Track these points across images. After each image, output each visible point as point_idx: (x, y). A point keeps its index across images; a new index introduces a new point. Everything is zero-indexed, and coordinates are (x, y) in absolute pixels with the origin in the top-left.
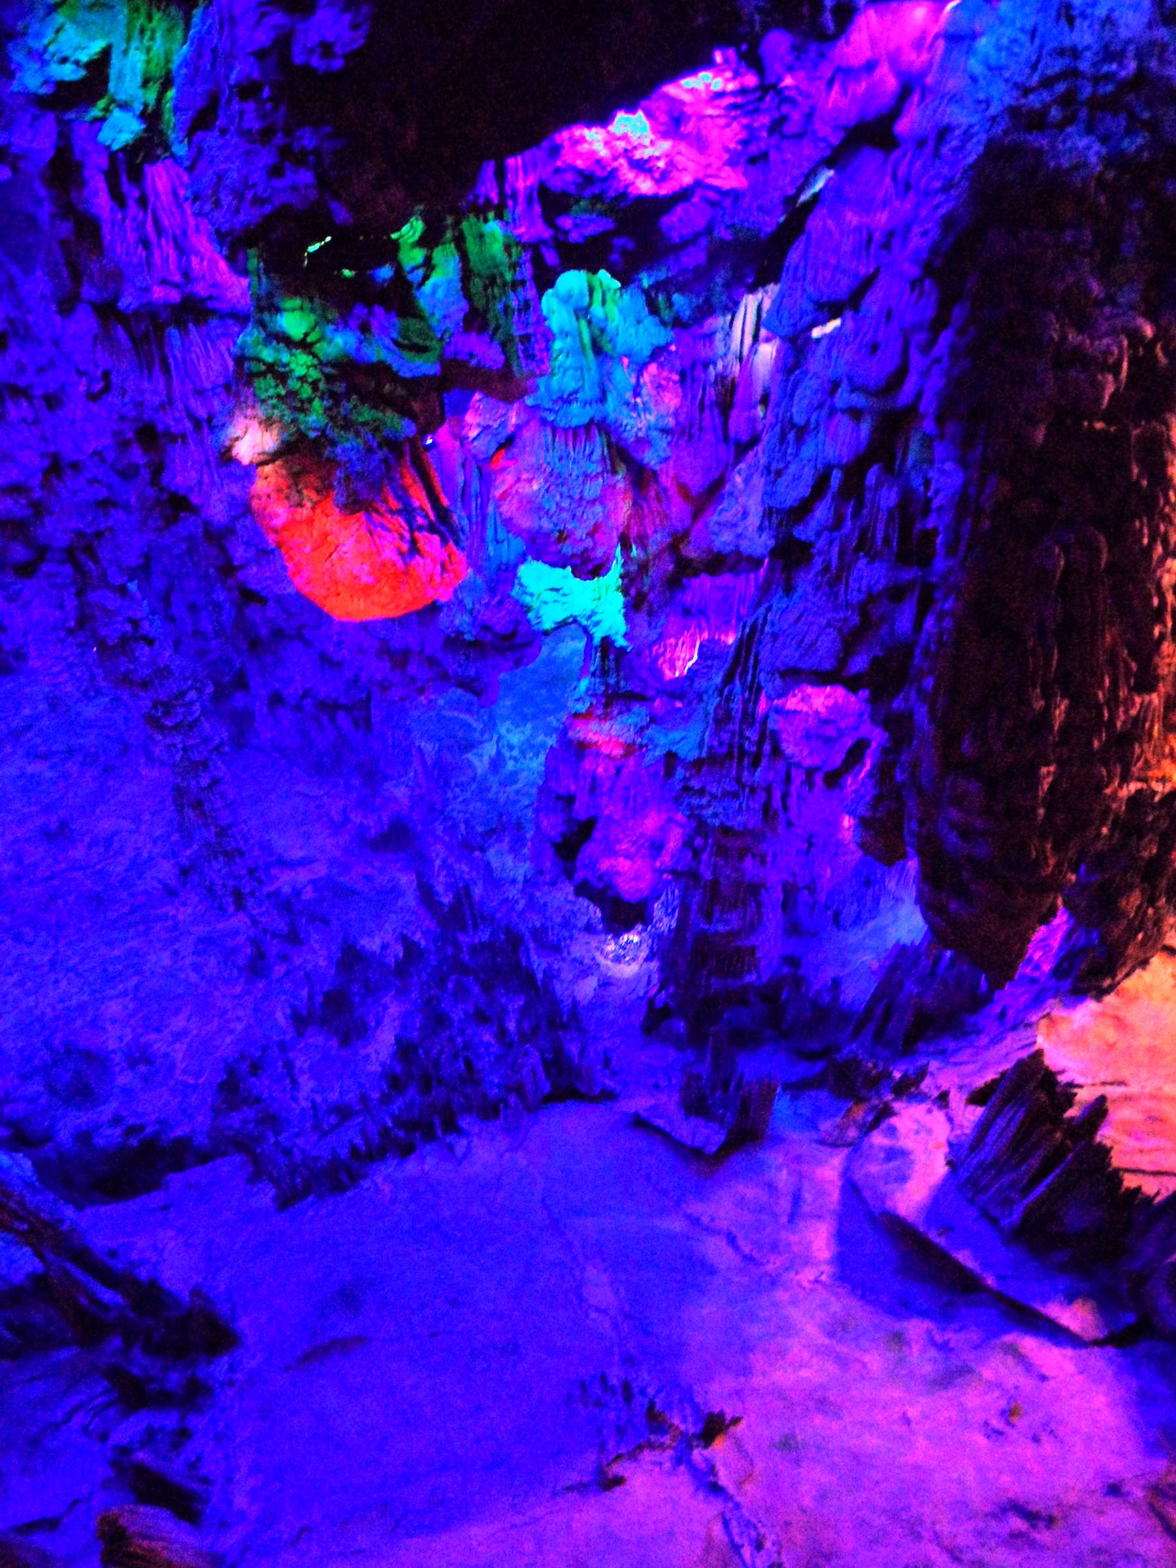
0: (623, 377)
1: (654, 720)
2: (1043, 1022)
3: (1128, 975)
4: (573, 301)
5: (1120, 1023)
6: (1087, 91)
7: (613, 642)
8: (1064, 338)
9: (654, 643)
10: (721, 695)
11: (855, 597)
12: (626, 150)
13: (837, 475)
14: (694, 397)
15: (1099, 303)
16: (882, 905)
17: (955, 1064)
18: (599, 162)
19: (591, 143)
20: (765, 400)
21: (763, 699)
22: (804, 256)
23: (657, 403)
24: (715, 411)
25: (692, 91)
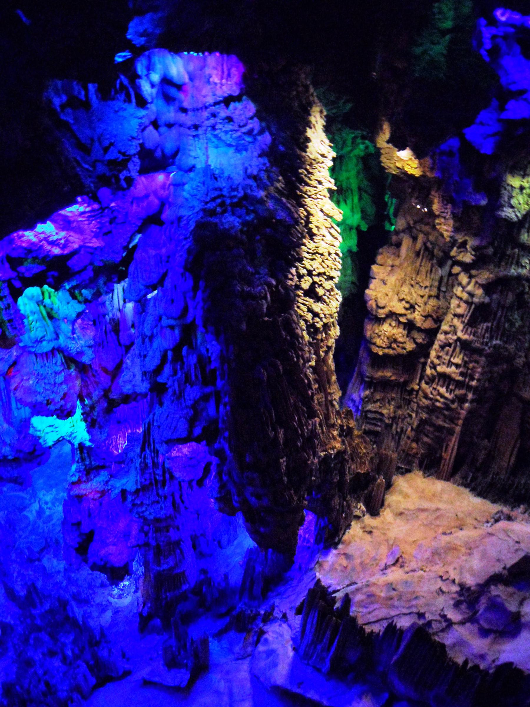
0: (66, 328)
1: (112, 476)
2: (317, 566)
3: (344, 534)
4: (35, 298)
5: (348, 556)
6: (228, 201)
7: (84, 444)
8: (243, 290)
9: (105, 440)
10: (141, 457)
11: (189, 403)
12: (45, 238)
13: (170, 353)
14: (102, 330)
15: (253, 274)
16: (238, 532)
17: (286, 598)
18: (33, 243)
19: (28, 236)
20: (133, 326)
21: (160, 455)
22: (136, 268)
23: (84, 336)
24: (112, 336)
25: (71, 212)
